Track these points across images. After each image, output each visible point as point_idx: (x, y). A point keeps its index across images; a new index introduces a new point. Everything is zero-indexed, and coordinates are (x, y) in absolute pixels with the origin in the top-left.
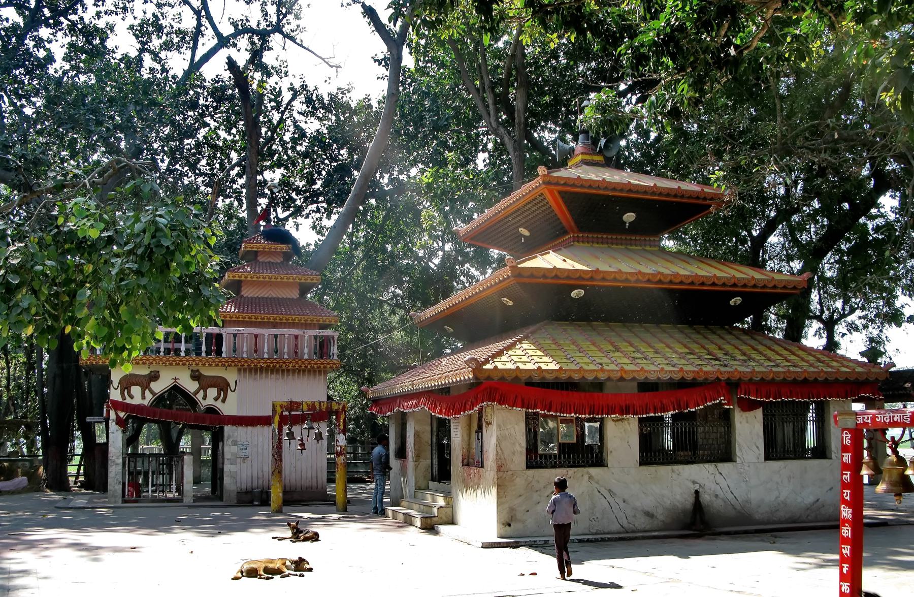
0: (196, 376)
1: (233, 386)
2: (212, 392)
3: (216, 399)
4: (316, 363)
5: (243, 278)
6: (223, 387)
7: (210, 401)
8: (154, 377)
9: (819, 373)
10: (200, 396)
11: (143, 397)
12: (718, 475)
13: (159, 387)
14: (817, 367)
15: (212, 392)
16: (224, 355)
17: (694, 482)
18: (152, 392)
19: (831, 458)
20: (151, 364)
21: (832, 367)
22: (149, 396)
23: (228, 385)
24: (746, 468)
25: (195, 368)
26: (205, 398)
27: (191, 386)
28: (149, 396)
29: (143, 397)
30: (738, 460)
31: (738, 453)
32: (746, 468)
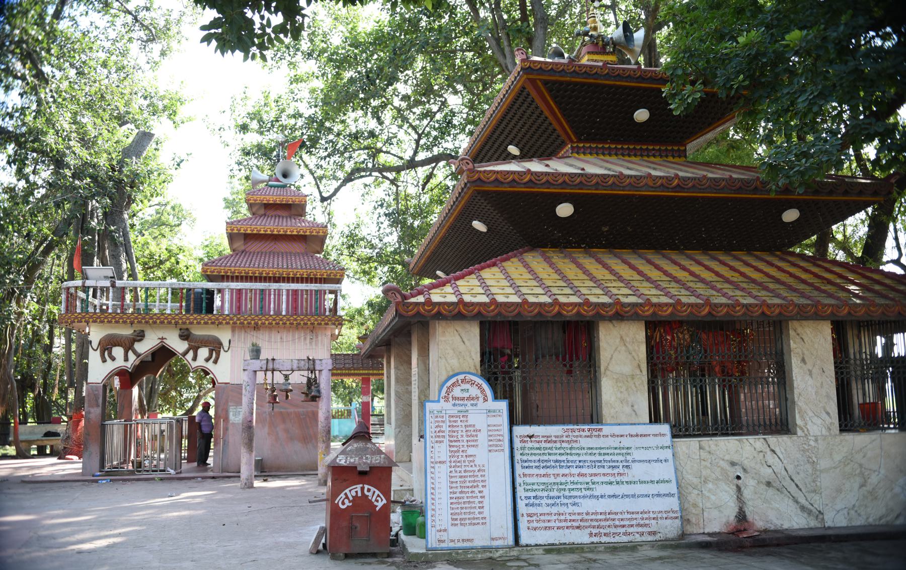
0: (185, 336)
1: (226, 344)
2: (203, 352)
3: (207, 360)
4: (274, 320)
5: (308, 233)
6: (215, 347)
7: (200, 362)
8: (140, 336)
9: (734, 306)
10: (190, 355)
11: (126, 359)
12: (769, 453)
13: (144, 347)
14: (784, 298)
16: (215, 312)
17: (733, 464)
18: (135, 352)
19: (795, 434)
20: (132, 323)
21: (838, 298)
22: (132, 357)
23: (221, 344)
24: (812, 443)
25: (184, 327)
26: (195, 359)
27: (179, 346)
28: (132, 357)
29: (126, 359)
30: (799, 432)
31: (799, 422)
32: (812, 443)
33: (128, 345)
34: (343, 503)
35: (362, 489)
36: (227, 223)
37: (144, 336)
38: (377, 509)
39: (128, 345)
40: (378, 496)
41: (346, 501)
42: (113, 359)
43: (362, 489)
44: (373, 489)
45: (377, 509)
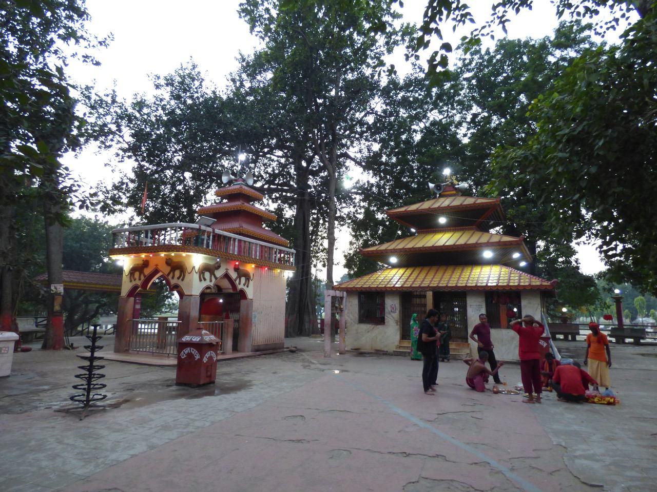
11: (211, 281)
15: (243, 279)
29: (211, 281)
42: (205, 280)
44: (195, 350)
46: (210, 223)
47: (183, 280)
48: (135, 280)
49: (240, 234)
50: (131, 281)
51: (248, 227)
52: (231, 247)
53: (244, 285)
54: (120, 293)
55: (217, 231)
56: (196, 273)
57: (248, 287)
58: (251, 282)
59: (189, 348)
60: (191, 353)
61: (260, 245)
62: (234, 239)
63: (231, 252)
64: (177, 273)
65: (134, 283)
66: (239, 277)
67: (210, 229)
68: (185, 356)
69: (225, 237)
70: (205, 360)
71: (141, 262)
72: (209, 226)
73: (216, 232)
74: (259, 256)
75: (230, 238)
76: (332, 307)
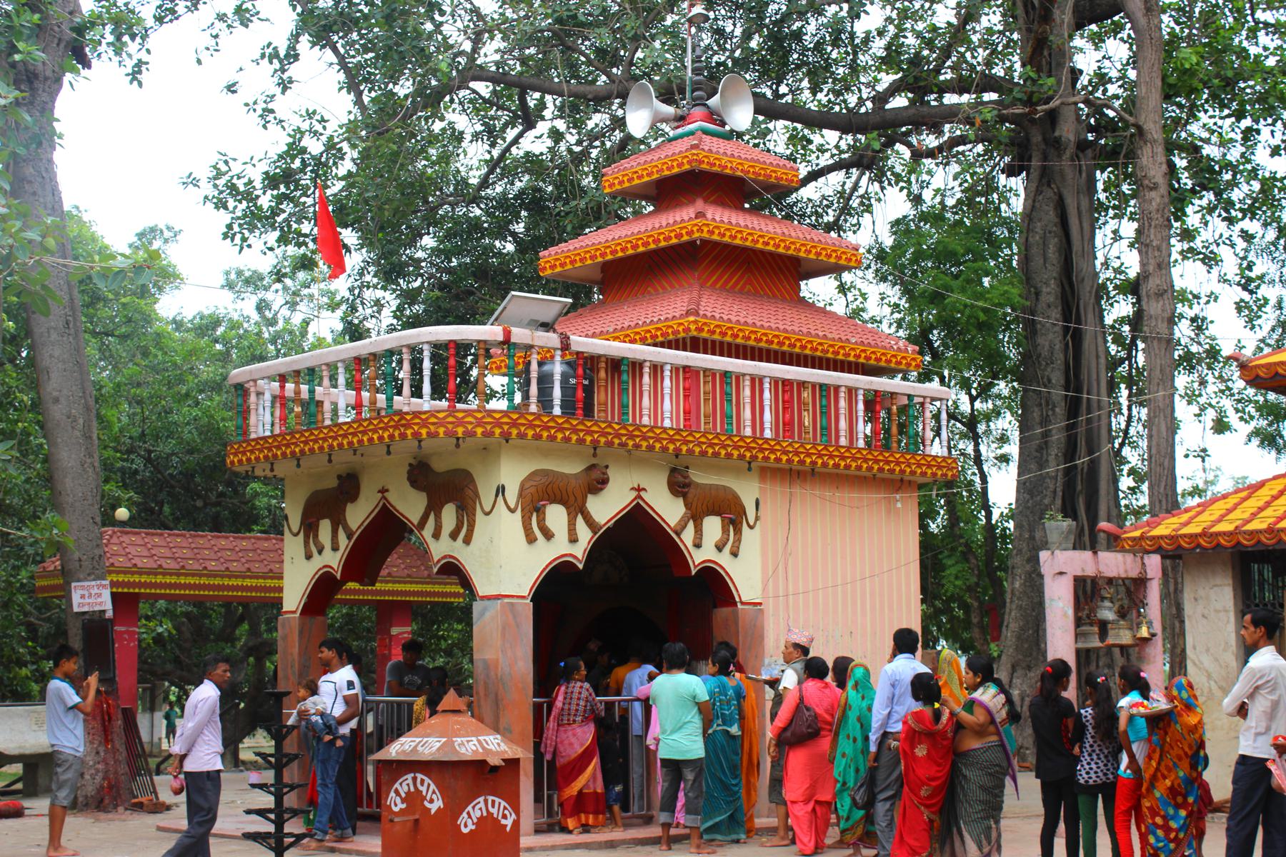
0: (679, 486)
8: (597, 483)
11: (573, 539)
15: (713, 526)
27: (669, 510)
29: (573, 539)
33: (574, 498)
34: (466, 826)
35: (415, 779)
36: (410, 465)
37: (604, 482)
38: (508, 829)
39: (574, 498)
40: (505, 808)
41: (469, 822)
42: (548, 535)
43: (415, 779)
44: (427, 780)
45: (508, 829)
46: (548, 314)
47: (467, 541)
48: (320, 552)
49: (695, 345)
50: (309, 557)
51: (724, 310)
52: (646, 401)
53: (720, 548)
54: (278, 603)
55: (583, 343)
56: (512, 511)
57: (735, 554)
58: (750, 538)
59: (481, 799)
60: (418, 792)
61: (775, 382)
62: (657, 369)
63: (646, 420)
64: (449, 515)
65: (318, 562)
66: (696, 515)
67: (552, 339)
68: (471, 827)
69: (615, 364)
70: (467, 824)
71: (332, 483)
72: (547, 326)
73: (574, 348)
74: (563, 406)
75: (636, 366)
76: (1078, 622)
